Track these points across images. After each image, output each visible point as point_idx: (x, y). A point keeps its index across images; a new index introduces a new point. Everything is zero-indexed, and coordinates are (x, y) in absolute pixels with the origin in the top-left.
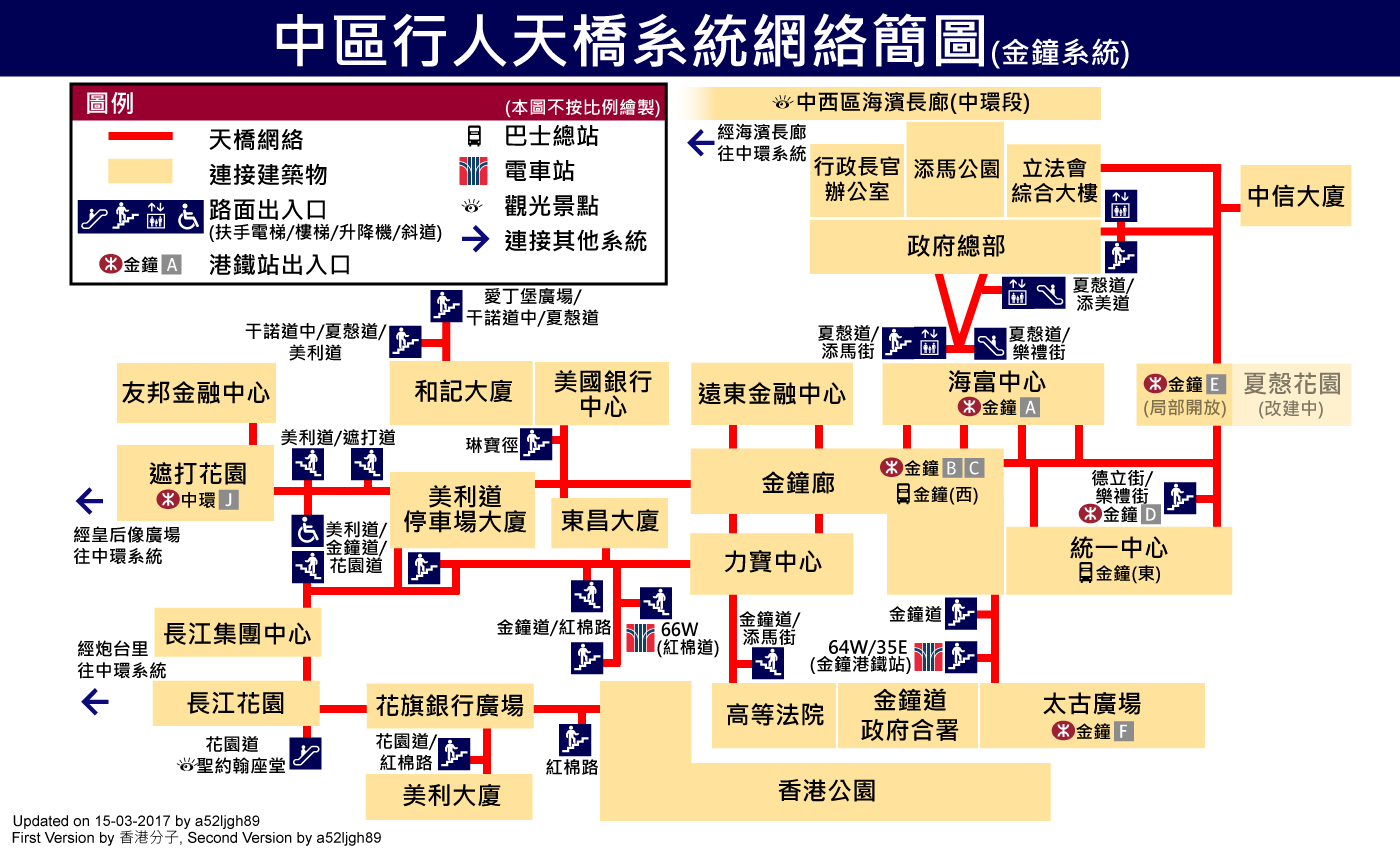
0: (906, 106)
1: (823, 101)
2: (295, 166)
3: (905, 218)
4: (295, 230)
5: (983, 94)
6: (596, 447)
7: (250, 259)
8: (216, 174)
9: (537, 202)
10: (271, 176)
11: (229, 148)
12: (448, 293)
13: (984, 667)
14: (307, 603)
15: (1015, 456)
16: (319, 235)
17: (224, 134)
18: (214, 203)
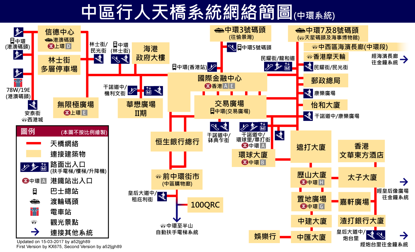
0: (351, 48)
1: (326, 47)
2: (76, 151)
4: (76, 170)
5: (374, 45)
7: (63, 179)
8: (52, 154)
9: (60, 221)
10: (69, 154)
11: (56, 146)
15: (35, 34)
16: (83, 172)
17: (55, 142)
18: (52, 163)
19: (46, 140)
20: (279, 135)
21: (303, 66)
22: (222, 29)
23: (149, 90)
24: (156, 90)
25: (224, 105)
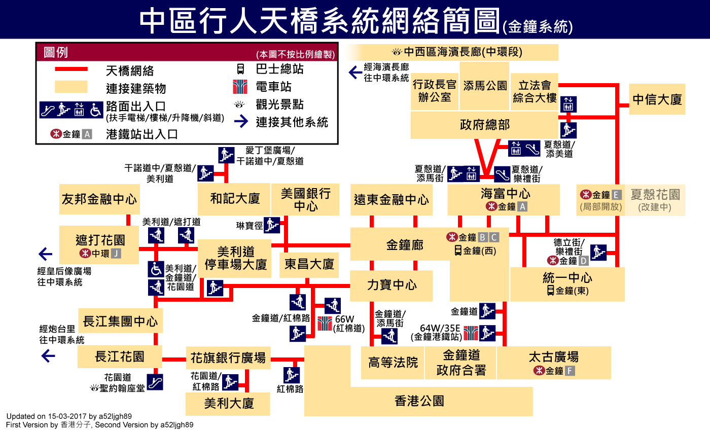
0: (459, 54)
1: (418, 51)
2: (150, 84)
3: (459, 110)
4: (150, 116)
5: (499, 48)
6: (302, 227)
7: (127, 132)
8: (109, 88)
9: (273, 103)
10: (138, 89)
11: (116, 75)
12: (227, 149)
13: (499, 338)
14: (156, 306)
15: (515, 231)
16: (162, 119)
17: (113, 68)
18: (109, 103)
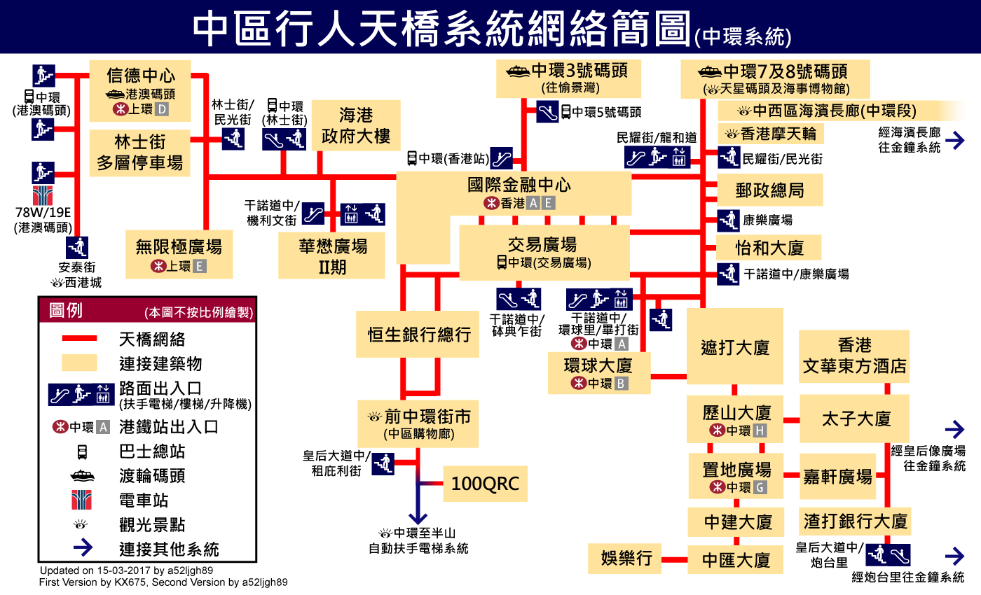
0: (830, 113)
1: (772, 110)
2: (180, 357)
4: (179, 402)
5: (884, 105)
7: (148, 423)
8: (124, 363)
9: (142, 522)
10: (163, 365)
11: (133, 345)
16: (196, 406)
17: (129, 335)
18: (123, 384)
19: (109, 332)
20: (659, 319)
21: (717, 156)
22: (524, 70)
23: (353, 211)
24: (369, 213)
25: (530, 247)
